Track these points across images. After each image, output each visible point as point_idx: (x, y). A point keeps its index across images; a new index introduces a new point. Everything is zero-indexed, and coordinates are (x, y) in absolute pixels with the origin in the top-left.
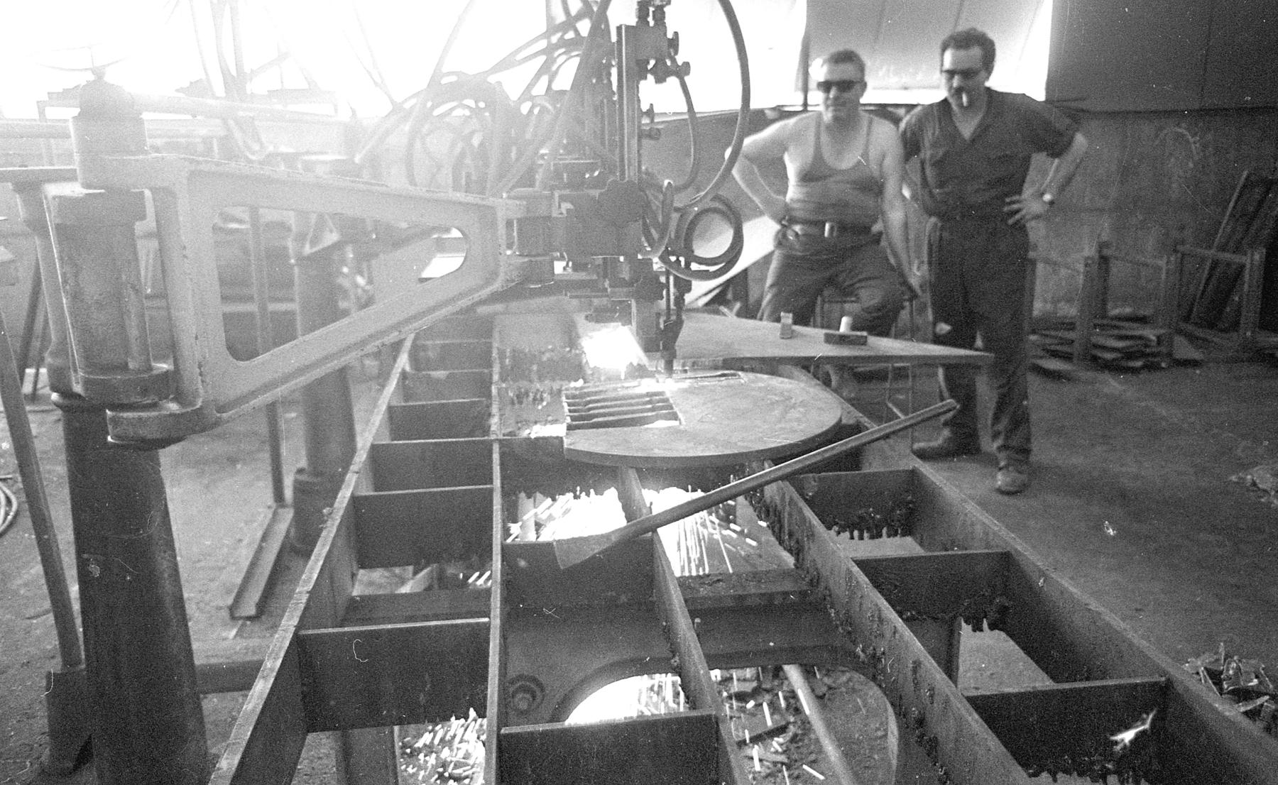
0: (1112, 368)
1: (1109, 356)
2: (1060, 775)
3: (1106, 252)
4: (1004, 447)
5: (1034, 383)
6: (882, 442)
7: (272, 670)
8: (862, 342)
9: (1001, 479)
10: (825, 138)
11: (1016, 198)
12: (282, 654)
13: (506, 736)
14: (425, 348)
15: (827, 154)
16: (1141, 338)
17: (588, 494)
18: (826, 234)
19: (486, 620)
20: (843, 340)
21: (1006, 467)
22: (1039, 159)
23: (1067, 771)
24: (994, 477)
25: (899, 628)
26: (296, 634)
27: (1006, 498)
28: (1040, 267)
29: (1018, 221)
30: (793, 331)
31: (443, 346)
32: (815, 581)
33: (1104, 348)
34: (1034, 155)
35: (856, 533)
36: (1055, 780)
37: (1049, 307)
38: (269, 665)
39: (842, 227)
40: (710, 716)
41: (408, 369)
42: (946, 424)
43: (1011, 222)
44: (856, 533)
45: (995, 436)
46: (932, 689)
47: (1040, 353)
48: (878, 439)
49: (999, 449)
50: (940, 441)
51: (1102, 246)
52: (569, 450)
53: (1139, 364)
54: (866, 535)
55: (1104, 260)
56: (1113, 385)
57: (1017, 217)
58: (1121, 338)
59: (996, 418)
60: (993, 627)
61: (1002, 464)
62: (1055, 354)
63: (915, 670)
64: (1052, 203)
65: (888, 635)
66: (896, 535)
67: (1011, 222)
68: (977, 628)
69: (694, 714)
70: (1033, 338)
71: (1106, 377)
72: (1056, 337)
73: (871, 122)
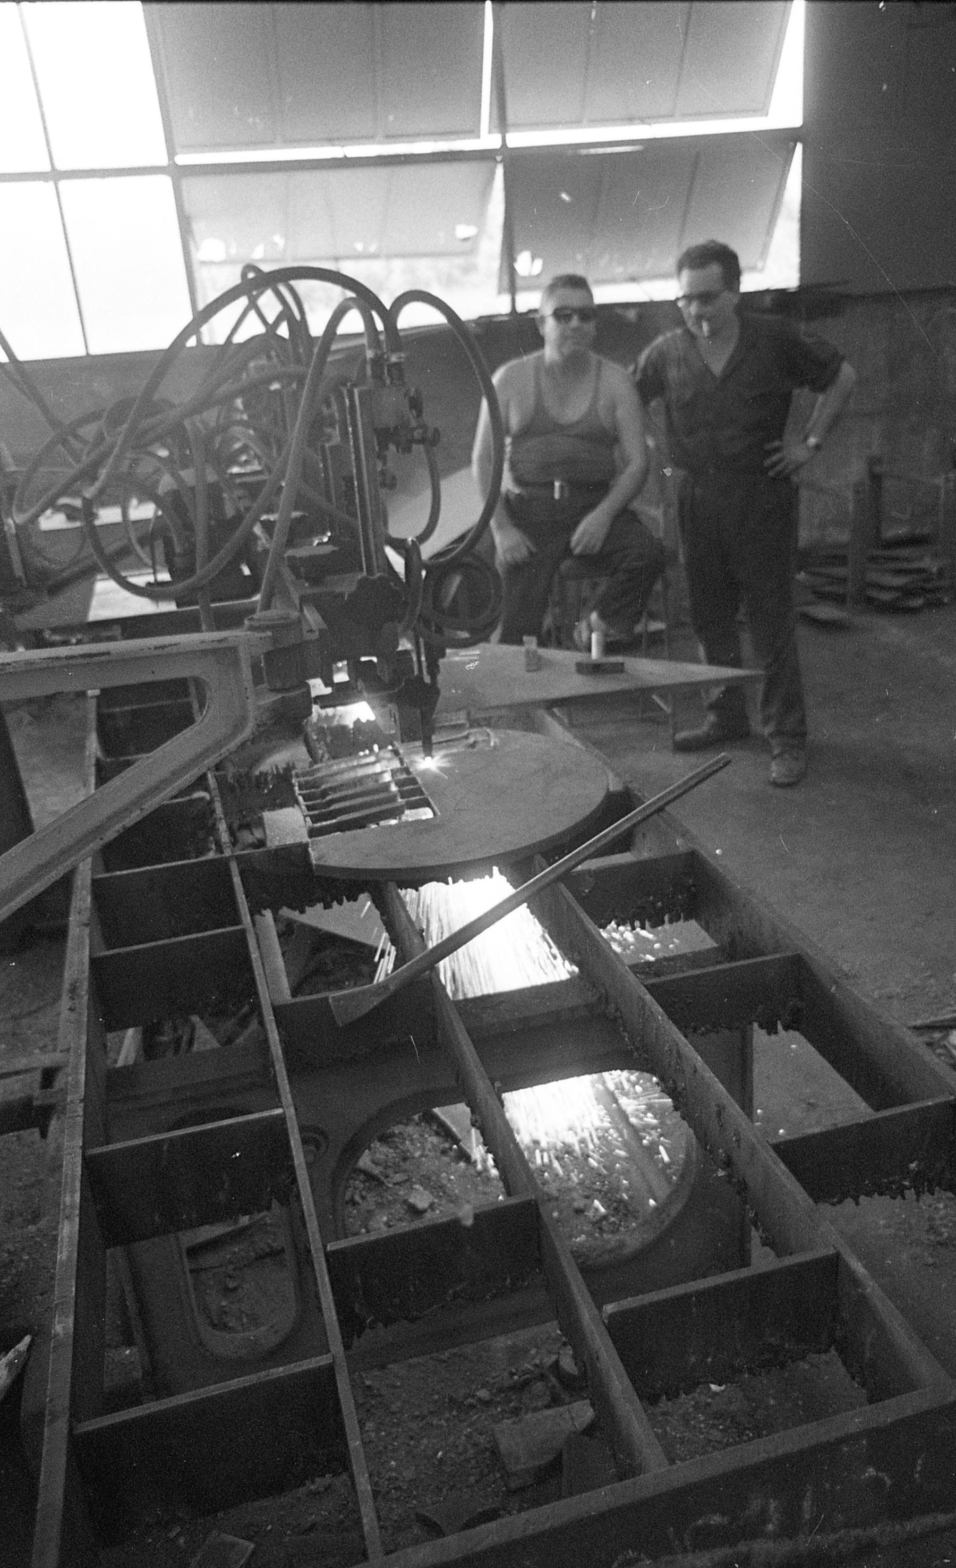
0: (892, 609)
1: (886, 596)
2: (863, 1199)
3: (877, 469)
4: (778, 733)
5: (802, 632)
6: (656, 816)
7: (72, 1207)
8: (619, 669)
9: (776, 770)
10: (545, 382)
11: (776, 444)
12: (78, 1184)
13: (333, 1252)
14: (111, 716)
15: (550, 403)
16: (920, 571)
17: (340, 903)
18: (557, 495)
19: (279, 1111)
20: (595, 669)
21: (780, 755)
22: (801, 395)
23: (869, 1194)
24: (768, 768)
25: (700, 1069)
26: (84, 1158)
27: (780, 792)
28: (804, 494)
29: (780, 472)
30: (540, 658)
31: (134, 713)
32: (605, 999)
33: (882, 588)
34: (796, 392)
35: (637, 923)
36: (857, 1204)
37: (816, 534)
38: (68, 1199)
39: (573, 485)
40: (531, 1200)
41: (99, 754)
42: (711, 707)
43: (771, 474)
44: (637, 923)
45: (766, 721)
46: (737, 1134)
47: (811, 597)
48: (652, 814)
49: (771, 735)
50: (705, 728)
51: (873, 462)
52: (317, 866)
53: (918, 602)
54: (647, 924)
55: (876, 479)
56: (893, 632)
57: (778, 468)
58: (899, 572)
59: (766, 701)
60: (786, 1028)
61: (776, 752)
62: (823, 597)
63: (719, 1114)
64: (818, 447)
65: (688, 1070)
66: (678, 919)
67: (771, 474)
68: (771, 1029)
69: (513, 1201)
70: (801, 576)
71: (882, 622)
72: (828, 576)
73: (600, 363)
